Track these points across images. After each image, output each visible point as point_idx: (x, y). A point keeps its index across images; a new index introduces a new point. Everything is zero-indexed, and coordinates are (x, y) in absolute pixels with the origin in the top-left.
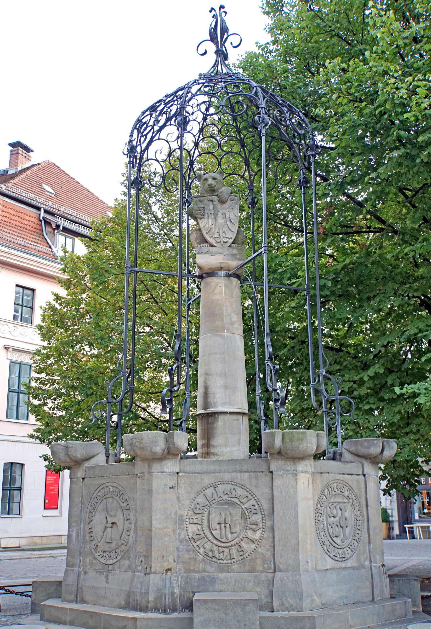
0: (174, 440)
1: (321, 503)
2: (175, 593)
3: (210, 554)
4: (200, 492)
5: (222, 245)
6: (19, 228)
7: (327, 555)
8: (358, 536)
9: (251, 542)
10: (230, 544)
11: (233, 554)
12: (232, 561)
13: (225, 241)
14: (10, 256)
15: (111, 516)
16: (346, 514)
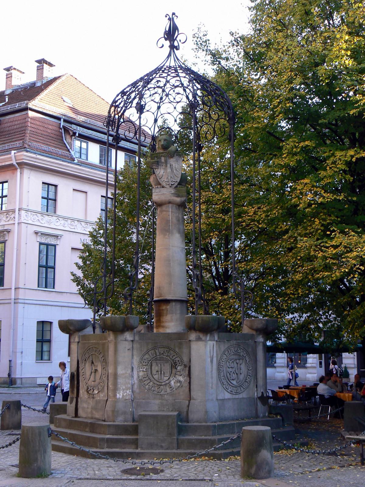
6: (44, 136)
13: (173, 183)
14: (37, 161)
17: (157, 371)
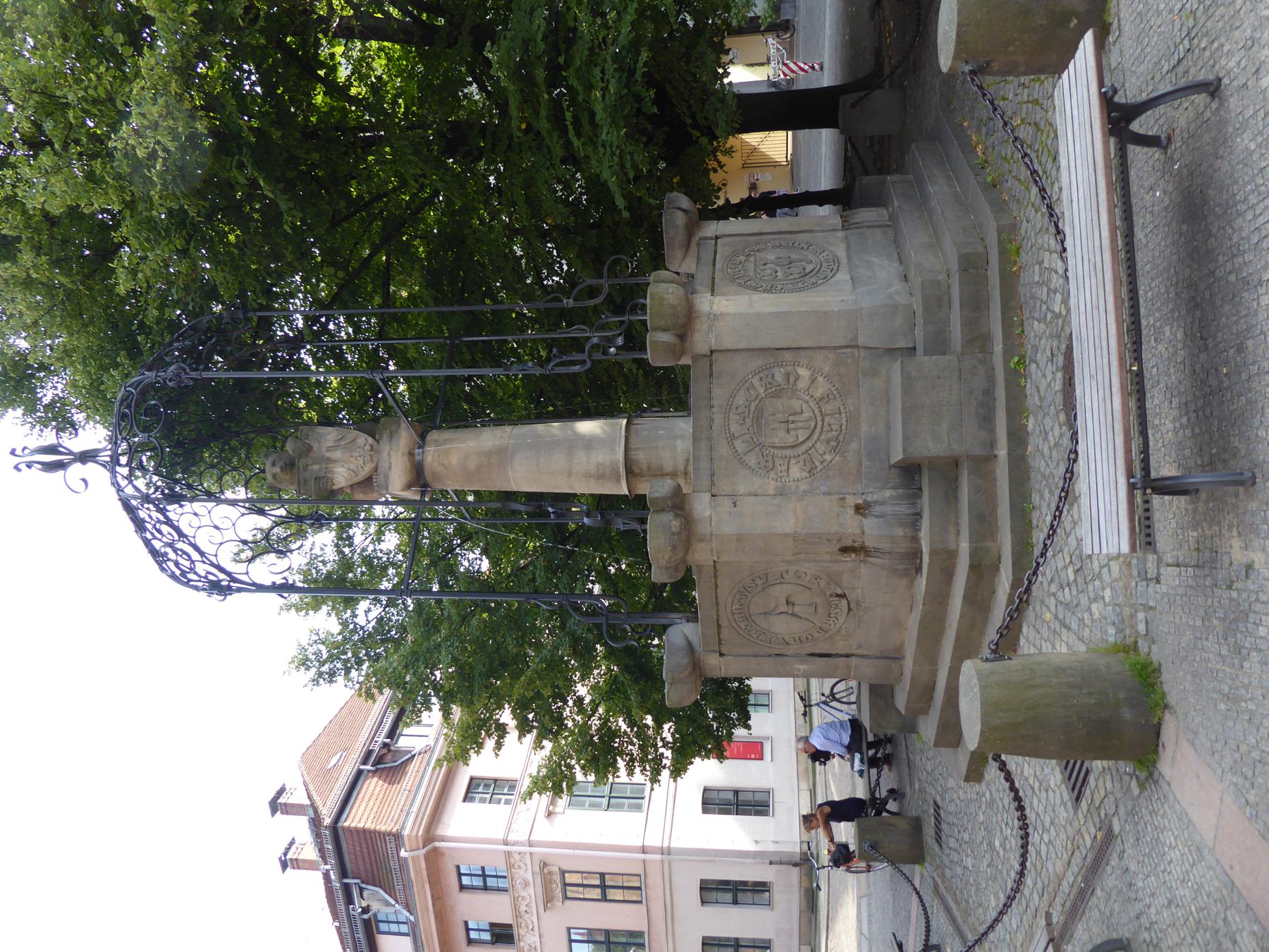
3: (833, 444)
10: (818, 414)
15: (777, 606)
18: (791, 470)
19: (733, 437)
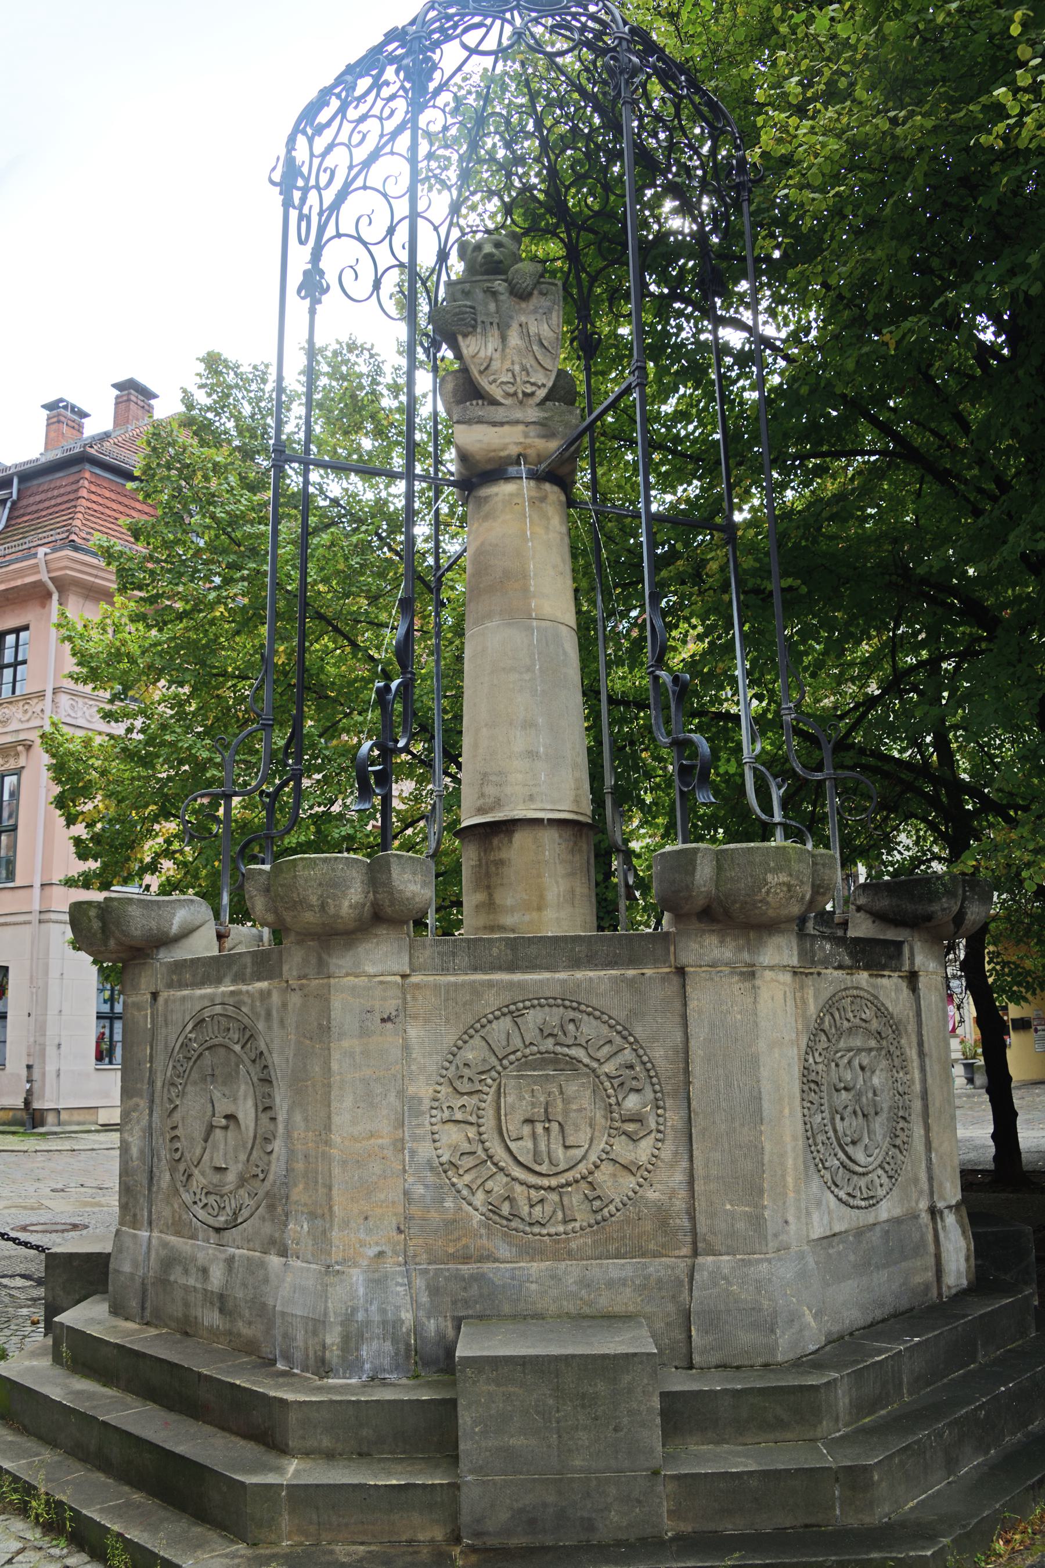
0: (390, 877)
1: (817, 1055)
2: (402, 1322)
3: (506, 1208)
4: (472, 1031)
5: (521, 402)
7: (831, 1196)
8: (903, 1136)
9: (625, 1173)
11: (571, 1208)
12: (570, 1227)
13: (529, 391)
16: (876, 1081)
17: (529, 1121)
18: (452, 1128)
19: (516, 1016)
